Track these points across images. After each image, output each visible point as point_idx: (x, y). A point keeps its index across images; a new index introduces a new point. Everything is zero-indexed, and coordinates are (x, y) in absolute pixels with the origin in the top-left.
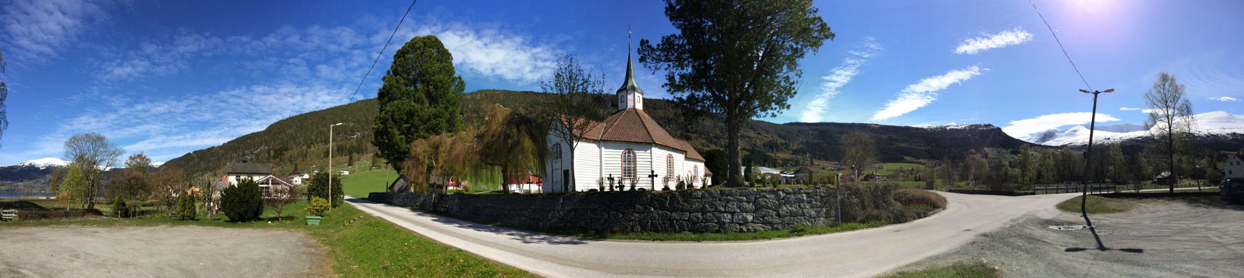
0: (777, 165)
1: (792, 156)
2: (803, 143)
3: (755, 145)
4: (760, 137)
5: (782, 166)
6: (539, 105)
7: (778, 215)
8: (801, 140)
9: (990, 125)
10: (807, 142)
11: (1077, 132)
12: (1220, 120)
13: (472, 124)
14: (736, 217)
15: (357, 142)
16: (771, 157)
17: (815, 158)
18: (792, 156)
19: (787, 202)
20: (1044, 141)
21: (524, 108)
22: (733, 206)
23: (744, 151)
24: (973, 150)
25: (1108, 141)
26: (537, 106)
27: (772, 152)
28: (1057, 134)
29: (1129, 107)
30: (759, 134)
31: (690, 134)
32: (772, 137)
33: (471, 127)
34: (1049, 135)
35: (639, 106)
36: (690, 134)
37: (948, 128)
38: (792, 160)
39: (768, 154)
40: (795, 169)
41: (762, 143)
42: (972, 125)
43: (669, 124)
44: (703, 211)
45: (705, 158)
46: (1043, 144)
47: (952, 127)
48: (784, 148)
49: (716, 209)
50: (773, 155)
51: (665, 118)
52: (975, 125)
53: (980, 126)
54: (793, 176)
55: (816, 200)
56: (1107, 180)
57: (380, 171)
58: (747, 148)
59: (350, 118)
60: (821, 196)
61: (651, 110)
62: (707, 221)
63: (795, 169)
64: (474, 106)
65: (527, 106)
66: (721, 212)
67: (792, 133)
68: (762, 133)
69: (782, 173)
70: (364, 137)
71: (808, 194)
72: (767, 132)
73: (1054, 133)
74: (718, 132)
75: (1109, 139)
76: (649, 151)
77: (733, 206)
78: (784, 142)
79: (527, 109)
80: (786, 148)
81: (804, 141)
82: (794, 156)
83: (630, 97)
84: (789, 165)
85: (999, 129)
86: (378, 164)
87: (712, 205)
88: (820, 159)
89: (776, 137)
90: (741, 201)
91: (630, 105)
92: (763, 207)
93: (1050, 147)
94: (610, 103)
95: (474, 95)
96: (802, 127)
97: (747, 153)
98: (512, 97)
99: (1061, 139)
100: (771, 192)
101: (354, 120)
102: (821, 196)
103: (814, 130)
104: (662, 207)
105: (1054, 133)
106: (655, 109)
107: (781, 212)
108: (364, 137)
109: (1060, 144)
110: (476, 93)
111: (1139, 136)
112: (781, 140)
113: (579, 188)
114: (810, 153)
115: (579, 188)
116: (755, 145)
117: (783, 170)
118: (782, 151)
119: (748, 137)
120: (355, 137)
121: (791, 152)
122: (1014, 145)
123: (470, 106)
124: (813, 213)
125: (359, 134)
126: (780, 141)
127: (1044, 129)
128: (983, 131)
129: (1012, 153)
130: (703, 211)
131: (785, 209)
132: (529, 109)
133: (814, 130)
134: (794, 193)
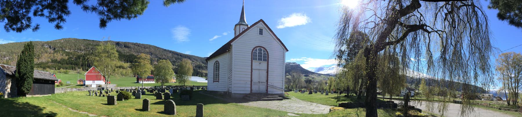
0: (203, 76)
4: (193, 62)
6: (90, 45)
9: (295, 63)
13: (60, 53)
15: (6, 61)
16: (200, 72)
20: (318, 71)
21: (83, 46)
26: (90, 46)
27: (200, 70)
28: (324, 68)
29: (172, 102)
30: (193, 61)
33: (59, 54)
34: (321, 69)
39: (199, 71)
46: (318, 73)
50: (201, 71)
52: (289, 63)
59: (4, 50)
61: (143, 49)
64: (60, 45)
65: (85, 45)
68: (194, 61)
70: (10, 59)
72: (197, 61)
74: (174, 59)
78: (205, 65)
79: (85, 47)
85: (299, 65)
89: (201, 63)
93: (322, 74)
94: (124, 46)
95: (60, 41)
98: (78, 41)
99: (327, 71)
101: (6, 51)
108: (10, 59)
109: (326, 73)
110: (61, 40)
112: (203, 64)
113: (164, 105)
115: (164, 105)
120: (6, 59)
122: (307, 73)
123: (58, 45)
125: (7, 58)
126: (203, 65)
127: (319, 66)
128: (292, 65)
129: (305, 76)
132: (86, 46)
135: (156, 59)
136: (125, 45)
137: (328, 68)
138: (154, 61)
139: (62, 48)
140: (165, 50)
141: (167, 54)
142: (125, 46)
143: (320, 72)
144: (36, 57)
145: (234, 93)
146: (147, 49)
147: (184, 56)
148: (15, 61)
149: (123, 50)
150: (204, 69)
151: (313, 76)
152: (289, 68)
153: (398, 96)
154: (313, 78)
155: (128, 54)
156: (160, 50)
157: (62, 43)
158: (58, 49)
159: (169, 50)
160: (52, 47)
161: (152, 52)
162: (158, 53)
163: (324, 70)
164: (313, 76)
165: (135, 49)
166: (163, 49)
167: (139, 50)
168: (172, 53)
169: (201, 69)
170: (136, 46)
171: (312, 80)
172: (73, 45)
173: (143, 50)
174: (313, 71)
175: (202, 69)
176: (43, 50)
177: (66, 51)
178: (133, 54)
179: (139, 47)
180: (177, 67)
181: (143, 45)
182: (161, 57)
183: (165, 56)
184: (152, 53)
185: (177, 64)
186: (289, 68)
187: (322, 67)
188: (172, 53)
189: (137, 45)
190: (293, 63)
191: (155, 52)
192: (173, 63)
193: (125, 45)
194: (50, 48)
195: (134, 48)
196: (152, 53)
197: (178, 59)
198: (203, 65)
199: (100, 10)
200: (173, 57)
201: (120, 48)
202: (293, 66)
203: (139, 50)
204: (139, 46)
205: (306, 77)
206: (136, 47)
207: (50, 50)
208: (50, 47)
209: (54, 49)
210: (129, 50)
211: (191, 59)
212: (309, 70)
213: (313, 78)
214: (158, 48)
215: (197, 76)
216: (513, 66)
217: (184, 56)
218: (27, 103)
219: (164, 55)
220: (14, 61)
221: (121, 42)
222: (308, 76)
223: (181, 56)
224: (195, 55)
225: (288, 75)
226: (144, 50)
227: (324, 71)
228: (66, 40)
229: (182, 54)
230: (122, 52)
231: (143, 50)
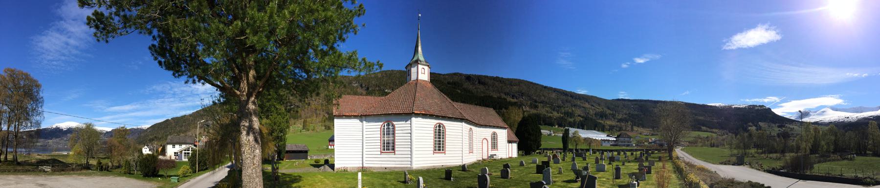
0: (605, 130)
1: (617, 124)
2: (626, 114)
3: (588, 113)
5: (609, 131)
8: (625, 111)
10: (629, 113)
11: (825, 113)
16: (600, 123)
17: (635, 125)
18: (617, 124)
23: (579, 117)
24: (750, 124)
25: (848, 119)
27: (602, 120)
28: (811, 113)
30: (592, 105)
32: (602, 109)
34: (803, 114)
37: (733, 107)
38: (617, 126)
40: (619, 133)
41: (594, 112)
42: (751, 106)
47: (737, 106)
48: (611, 117)
50: (603, 122)
51: (519, 92)
52: (753, 105)
53: (756, 106)
56: (868, 152)
57: (308, 132)
58: (582, 115)
61: (508, 86)
67: (618, 107)
68: (595, 105)
72: (599, 105)
73: (809, 113)
75: (848, 118)
78: (611, 112)
80: (613, 117)
81: (627, 112)
82: (618, 124)
86: (308, 127)
88: (638, 126)
94: (477, 81)
96: (626, 103)
97: (581, 119)
103: (635, 105)
105: (809, 113)
109: (813, 121)
111: (871, 115)
114: (631, 122)
116: (588, 113)
117: (609, 134)
118: (610, 119)
119: (583, 107)
121: (616, 120)
122: (782, 121)
126: (608, 112)
128: (758, 109)
129: (779, 127)
133: (635, 105)
135: (529, 103)
136: (479, 80)
137: (816, 112)
139: (379, 86)
140: (545, 87)
141: (549, 93)
142: (479, 83)
143: (805, 120)
145: (284, 174)
146: (515, 87)
147: (577, 97)
148: (308, 109)
149: (475, 88)
150: (610, 118)
151: (791, 126)
152: (753, 114)
154: (792, 129)
155: (482, 95)
157: (380, 78)
158: (373, 88)
159: (552, 88)
160: (364, 86)
161: (523, 91)
162: (533, 92)
163: (811, 115)
164: (791, 126)
165: (494, 87)
166: (542, 86)
168: (558, 91)
169: (604, 118)
170: (497, 81)
171: (790, 133)
172: (397, 82)
174: (793, 118)
175: (606, 119)
176: (351, 90)
177: (386, 91)
178: (492, 94)
180: (562, 115)
181: (508, 80)
182: (537, 99)
183: (545, 97)
186: (753, 114)
187: (807, 110)
188: (556, 92)
189: (498, 80)
190: (760, 106)
193: (479, 80)
194: (362, 87)
195: (493, 86)
198: (608, 112)
199: (95, 35)
200: (558, 99)
201: (471, 84)
202: (760, 110)
204: (501, 81)
205: (780, 129)
207: (361, 90)
208: (361, 86)
209: (368, 89)
210: (484, 88)
211: (589, 103)
212: (787, 117)
213: (791, 128)
214: (537, 84)
215: (595, 130)
219: (543, 96)
220: (306, 110)
221: (473, 75)
222: (784, 126)
223: (571, 96)
224: (598, 96)
225: (751, 126)
227: (811, 117)
228: (386, 74)
230: (473, 92)
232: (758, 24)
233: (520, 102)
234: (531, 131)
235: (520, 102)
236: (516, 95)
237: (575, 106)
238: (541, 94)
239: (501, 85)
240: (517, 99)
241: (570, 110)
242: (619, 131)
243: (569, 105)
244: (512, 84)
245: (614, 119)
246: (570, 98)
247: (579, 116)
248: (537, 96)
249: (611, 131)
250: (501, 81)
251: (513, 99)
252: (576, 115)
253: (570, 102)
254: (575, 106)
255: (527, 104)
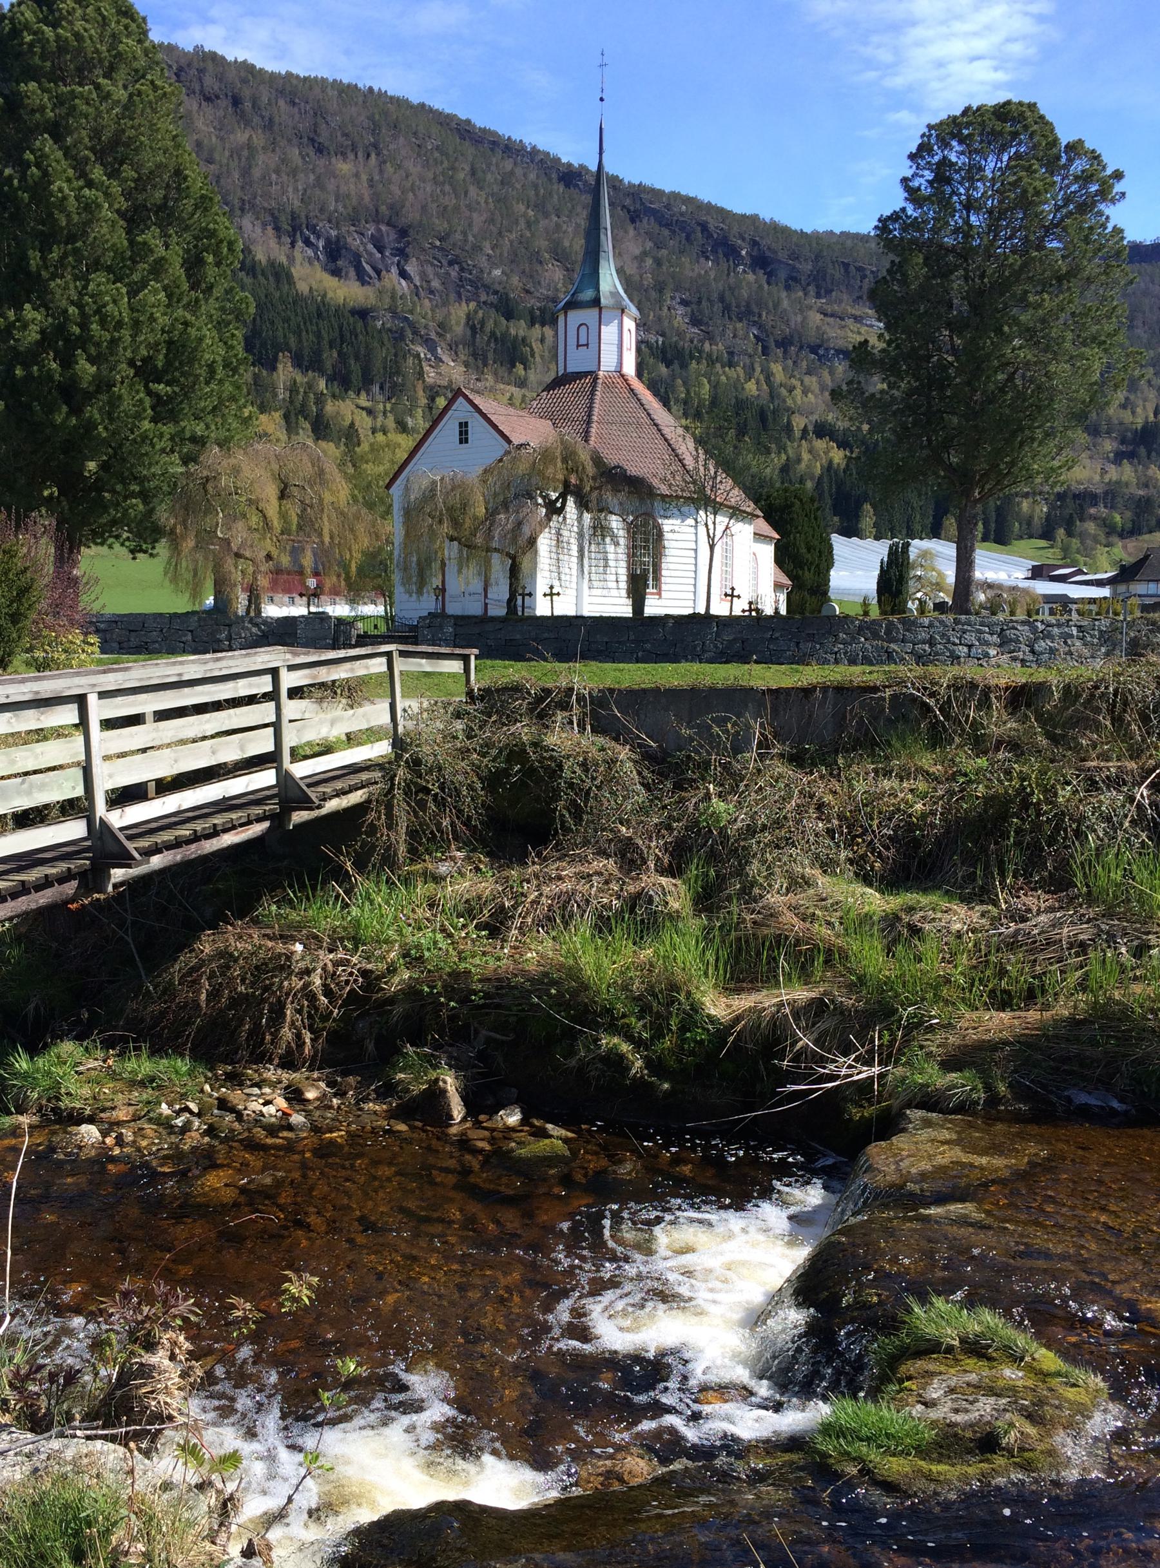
1: (1113, 473)
5: (1047, 534)
7: (1033, 652)
12: (306, 677)
14: (974, 650)
18: (1113, 473)
19: (1048, 636)
22: (970, 638)
23: (820, 444)
31: (518, 329)
35: (630, 368)
36: (518, 329)
38: (1111, 495)
40: (1125, 551)
43: (401, 253)
44: (931, 642)
45: (776, 528)
49: (949, 641)
51: (377, 219)
54: (1105, 592)
55: (1092, 636)
60: (1101, 631)
61: (294, 153)
62: (937, 654)
63: (1125, 551)
66: (954, 644)
69: (1037, 573)
71: (1079, 627)
76: (691, 521)
77: (970, 638)
82: (1127, 473)
83: (609, 332)
84: (1091, 527)
87: (943, 635)
90: (982, 632)
91: (608, 362)
92: (1011, 640)
97: (838, 456)
100: (1023, 623)
102: (1101, 631)
104: (876, 636)
106: (320, 150)
107: (1036, 647)
117: (1051, 556)
121: (1109, 445)
124: (1086, 652)
130: (931, 642)
131: (1041, 645)
134: (1059, 625)
135: (459, 312)
138: (431, 346)
144: (543, 223)
146: (344, 167)
153: (334, 647)
156: (506, 180)
161: (411, 215)
162: (478, 219)
167: (246, 172)
168: (654, 213)
173: (294, 173)
179: (244, 119)
184: (403, 233)
185: (706, 390)
188: (646, 224)
189: (209, 81)
191: (443, 211)
192: (663, 370)
196: (403, 233)
197: (727, 308)
203: (246, 172)
204: (236, 101)
206: (200, 124)
214: (510, 149)
216: (88, 396)
217: (806, 267)
218: (546, 1473)
223: (762, 262)
226: (306, 180)
229: (785, 231)
231: (294, 173)
232: (298, 299)
233: (393, 311)
234: (803, 550)
235: (393, 311)
236: (354, 242)
237: (784, 343)
238: (542, 243)
239: (241, 136)
240: (362, 278)
241: (751, 387)
242: (1133, 531)
243: (744, 336)
244: (324, 137)
245: (1094, 431)
246: (749, 279)
247: (822, 430)
248: (514, 259)
249: (1061, 532)
250: (236, 101)
251: (336, 273)
252: (799, 422)
253: (746, 314)
254: (784, 343)
255: (443, 326)
